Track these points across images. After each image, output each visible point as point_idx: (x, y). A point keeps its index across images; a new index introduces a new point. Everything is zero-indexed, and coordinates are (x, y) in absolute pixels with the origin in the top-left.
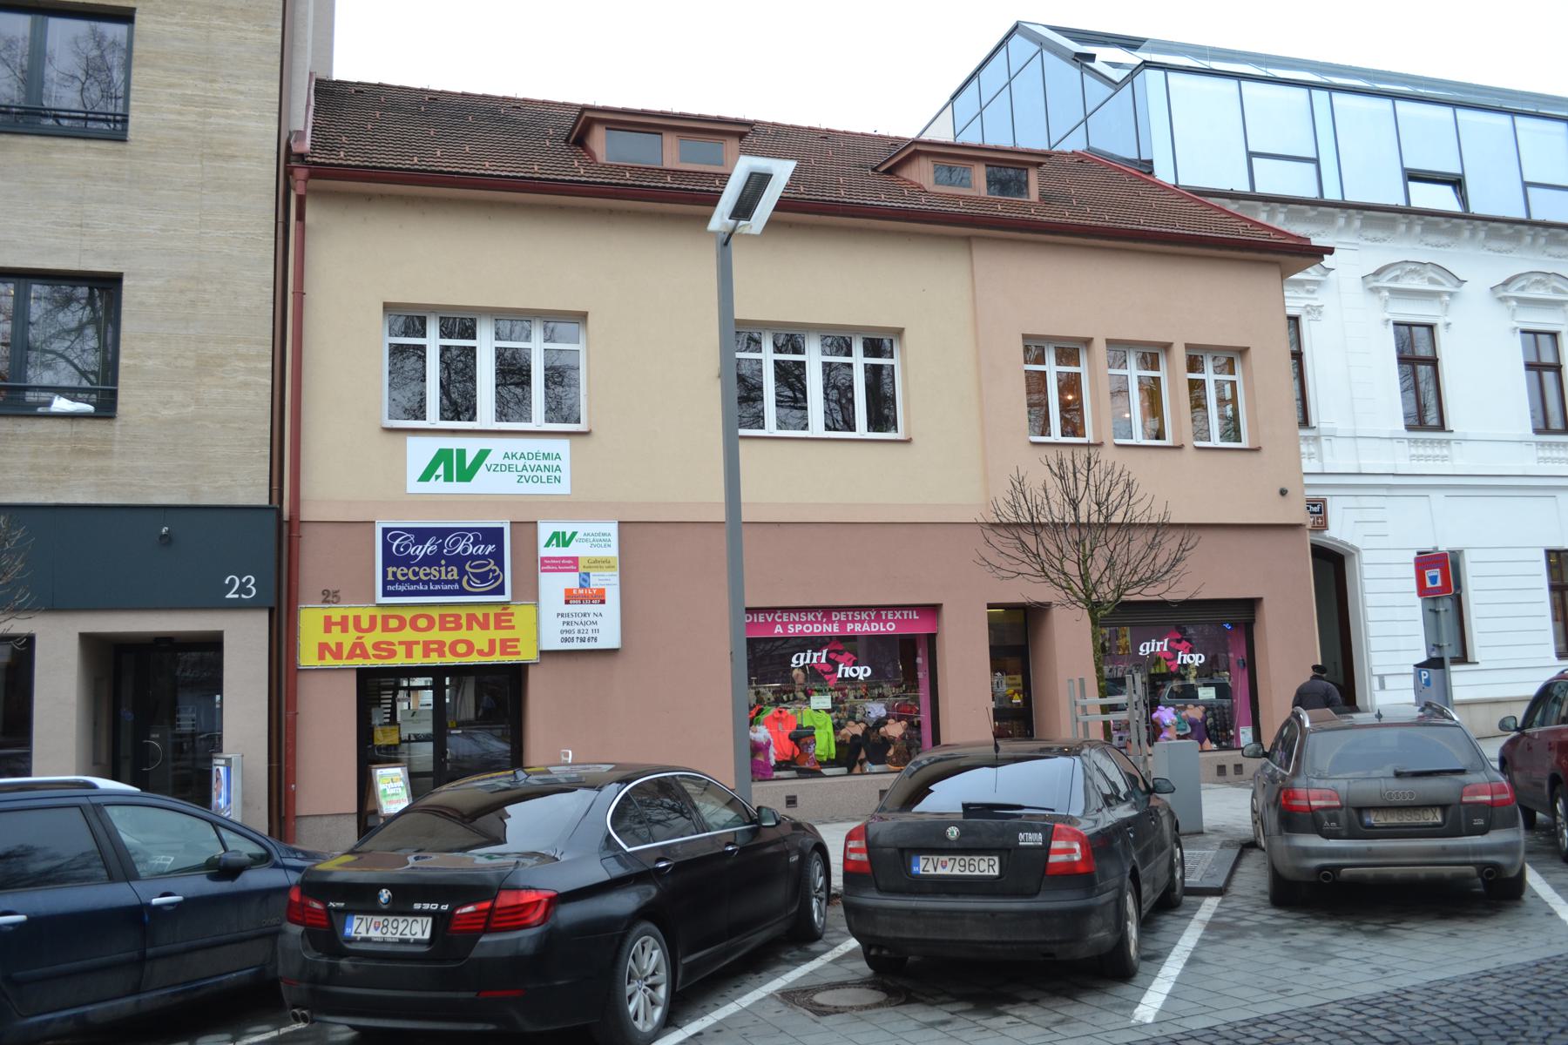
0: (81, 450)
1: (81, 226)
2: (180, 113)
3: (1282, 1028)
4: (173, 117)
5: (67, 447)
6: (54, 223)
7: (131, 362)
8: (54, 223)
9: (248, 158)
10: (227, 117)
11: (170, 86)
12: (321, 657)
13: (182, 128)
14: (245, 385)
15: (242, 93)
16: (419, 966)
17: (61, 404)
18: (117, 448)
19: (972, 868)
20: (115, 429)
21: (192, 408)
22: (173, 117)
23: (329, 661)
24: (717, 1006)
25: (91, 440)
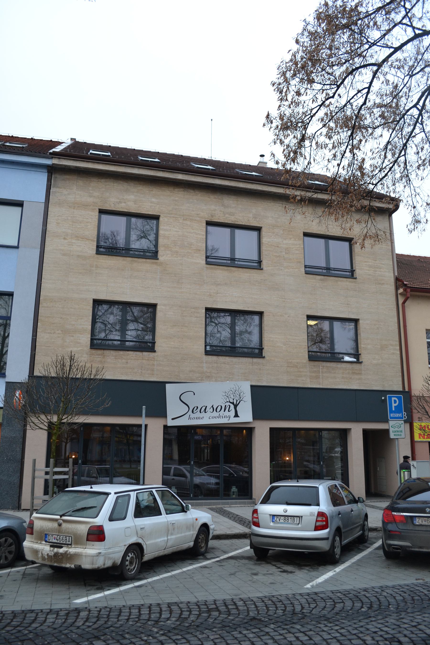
0: (354, 372)
1: (347, 304)
2: (369, 270)
3: (359, 632)
4: (367, 271)
5: (351, 372)
6: (341, 303)
7: (364, 346)
8: (341, 303)
9: (387, 284)
10: (380, 272)
11: (365, 262)
12: (420, 438)
13: (370, 275)
14: (393, 354)
15: (383, 264)
16: (355, 536)
17: (347, 358)
18: (363, 372)
19: (428, 522)
20: (362, 366)
21: (381, 361)
22: (367, 271)
23: (422, 439)
24: (125, 585)
25: (356, 369)
